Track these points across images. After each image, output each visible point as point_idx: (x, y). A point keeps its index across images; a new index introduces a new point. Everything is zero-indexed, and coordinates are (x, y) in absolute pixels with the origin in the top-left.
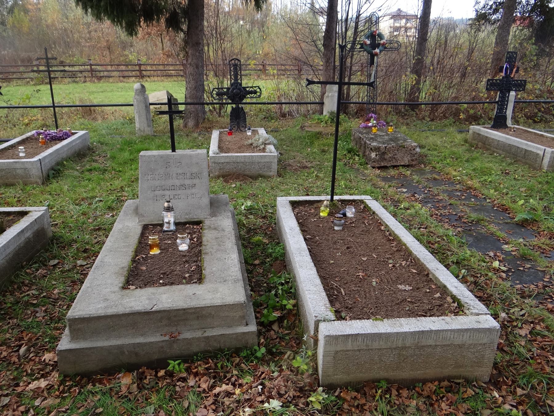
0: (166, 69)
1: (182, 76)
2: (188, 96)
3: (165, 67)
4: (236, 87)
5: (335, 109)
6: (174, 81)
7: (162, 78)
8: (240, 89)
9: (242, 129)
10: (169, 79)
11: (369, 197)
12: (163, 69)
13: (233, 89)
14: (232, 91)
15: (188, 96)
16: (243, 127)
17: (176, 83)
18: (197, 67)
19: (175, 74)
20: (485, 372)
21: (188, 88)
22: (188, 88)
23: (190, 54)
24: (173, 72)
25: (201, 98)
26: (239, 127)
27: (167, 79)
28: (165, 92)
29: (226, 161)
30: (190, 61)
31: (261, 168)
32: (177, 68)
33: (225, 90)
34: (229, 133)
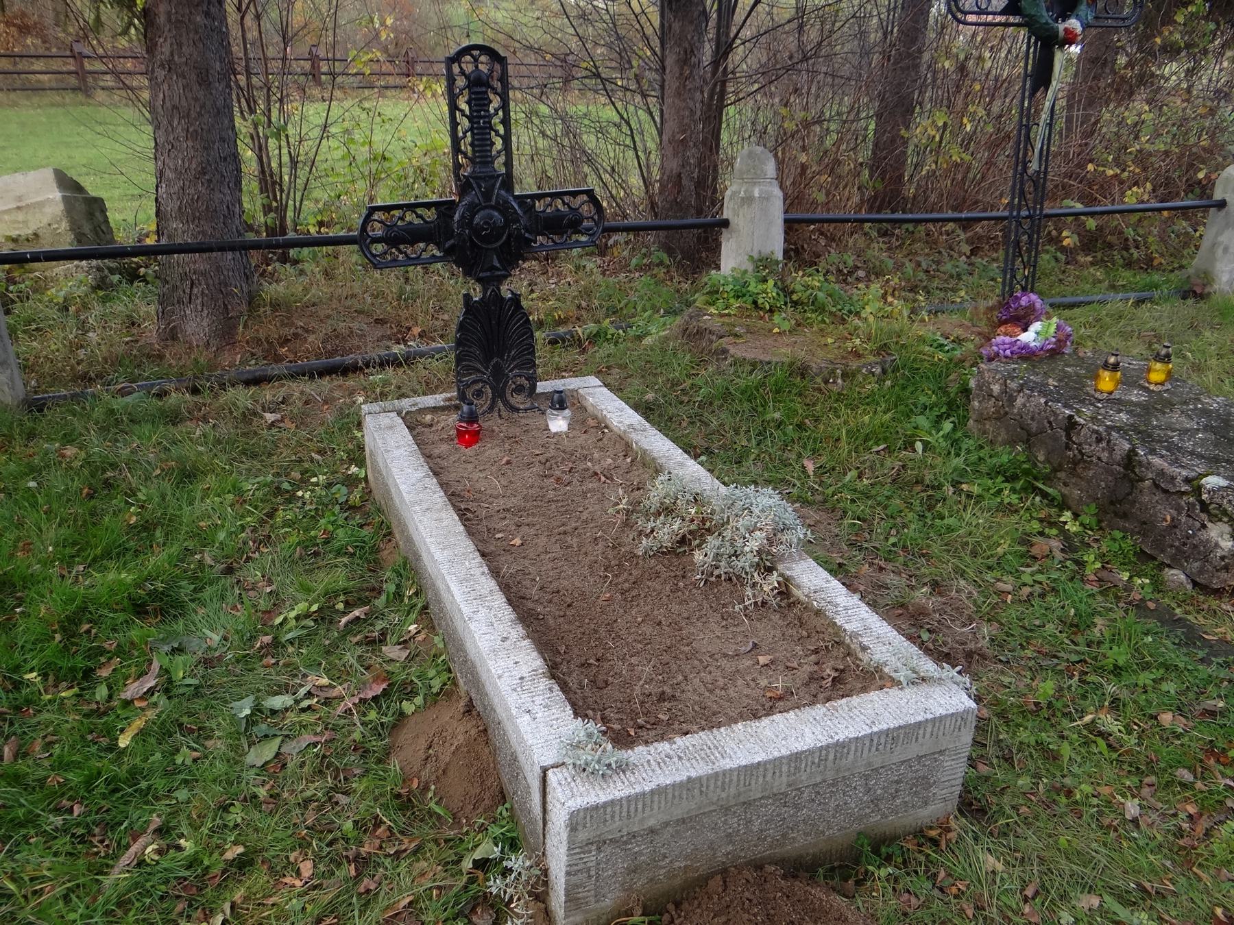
0: (20, 67)
1: (74, 89)
2: (170, 207)
3: (15, 64)
4: (487, 195)
5: (776, 245)
6: (53, 105)
7: (13, 96)
8: (503, 208)
9: (518, 400)
10: (36, 100)
11: (593, 381)
12: (10, 68)
13: (473, 209)
14: (466, 222)
15: (170, 207)
16: (519, 389)
17: (61, 110)
18: (204, 80)
19: (54, 85)
20: (939, 803)
21: (170, 174)
22: (170, 174)
23: (162, 19)
24: (46, 77)
25: (230, 215)
26: (499, 394)
27: (28, 98)
28: (49, 174)
29: (678, 813)
30: (164, 50)
31: (875, 801)
32: (56, 65)
33: (430, 215)
34: (460, 434)
